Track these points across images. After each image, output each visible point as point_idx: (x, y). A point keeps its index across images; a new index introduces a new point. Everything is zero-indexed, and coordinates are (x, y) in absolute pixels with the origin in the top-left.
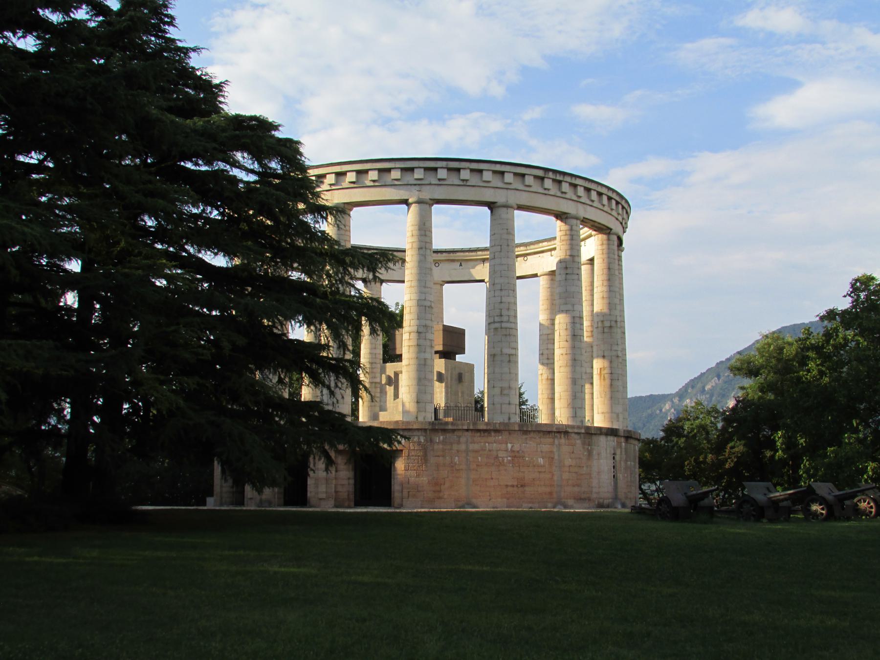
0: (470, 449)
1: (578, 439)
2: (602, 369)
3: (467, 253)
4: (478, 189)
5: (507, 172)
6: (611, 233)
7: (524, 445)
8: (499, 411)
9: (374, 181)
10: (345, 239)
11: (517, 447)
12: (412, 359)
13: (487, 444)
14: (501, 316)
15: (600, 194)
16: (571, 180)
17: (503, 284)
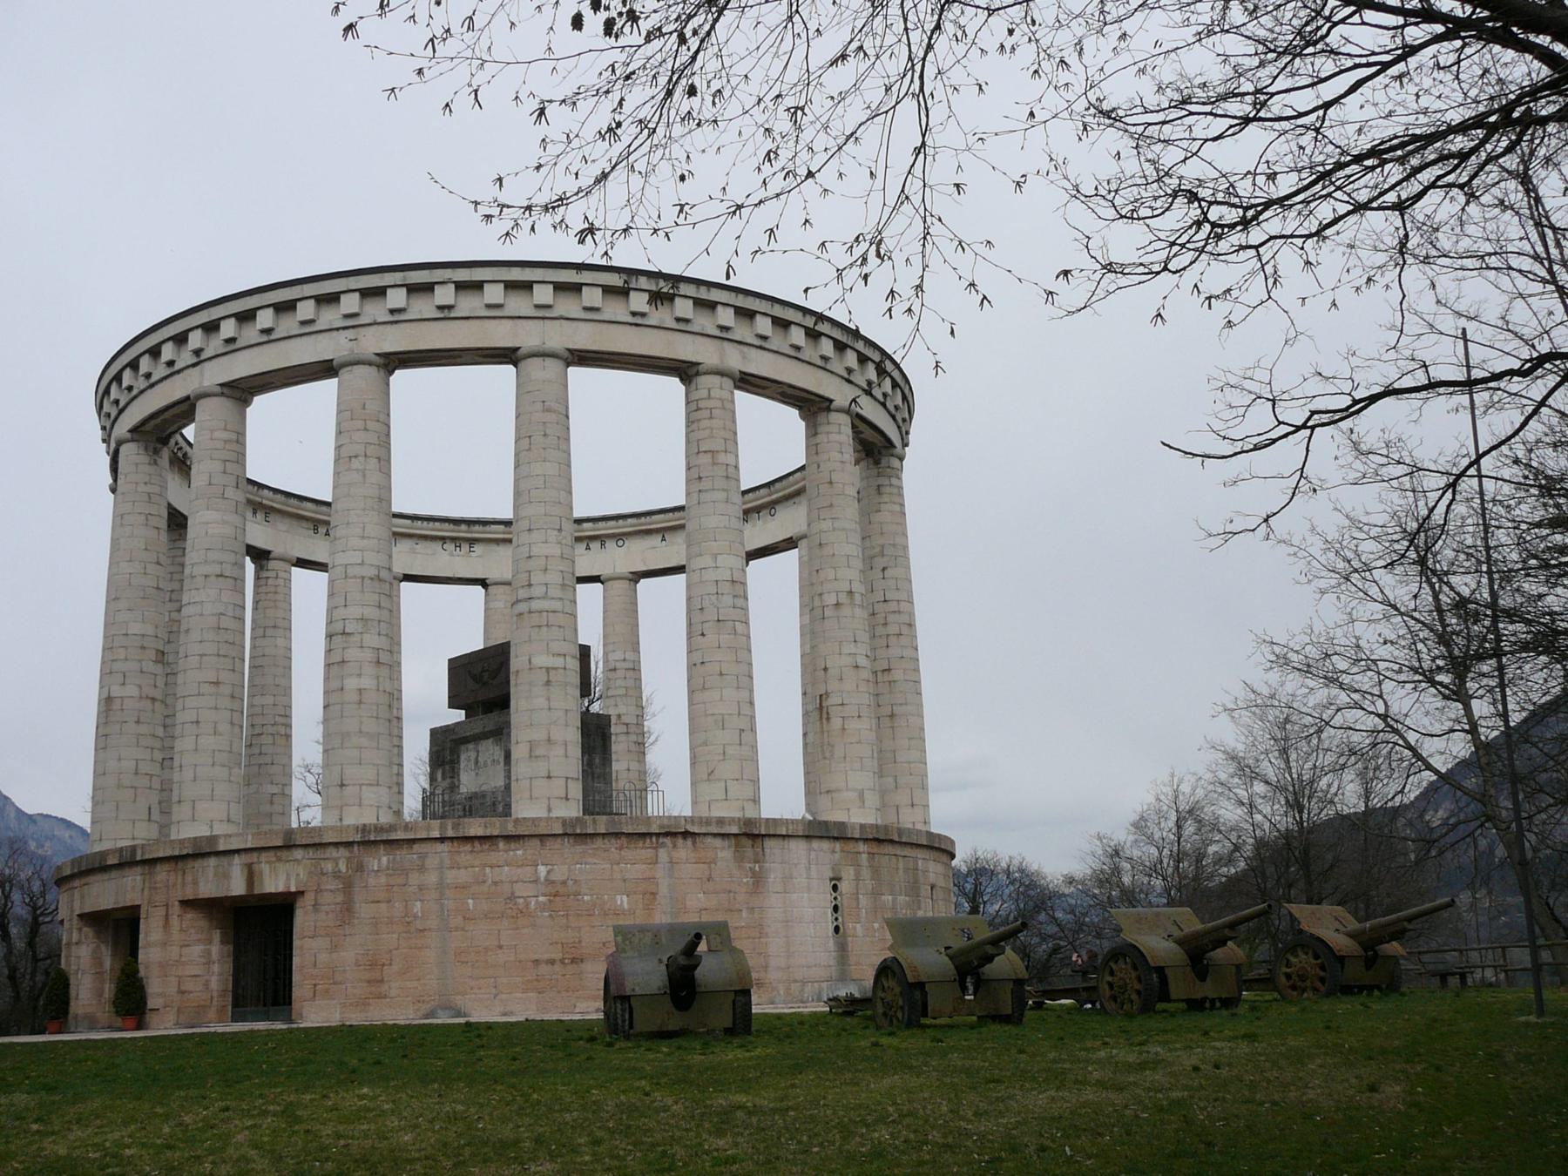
1: (723, 848)
6: (832, 407)
7: (578, 866)
8: (527, 795)
11: (560, 873)
13: (488, 870)
14: (530, 585)
16: (698, 292)
17: (533, 518)
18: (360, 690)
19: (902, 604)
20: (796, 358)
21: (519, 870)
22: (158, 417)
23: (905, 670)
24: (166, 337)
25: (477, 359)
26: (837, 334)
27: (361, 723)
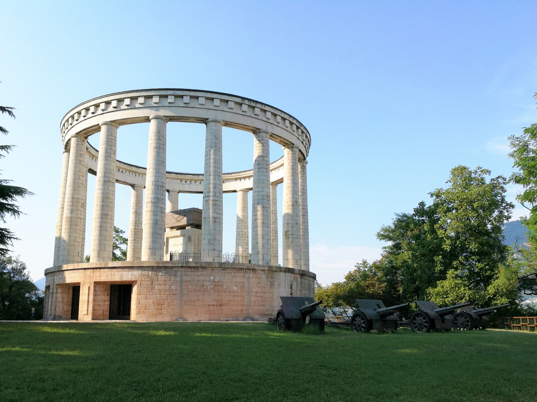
0: (184, 280)
1: (263, 274)
2: (287, 232)
3: (227, 175)
4: (196, 109)
5: (216, 98)
7: (223, 277)
8: (105, 230)
9: (128, 106)
10: (111, 144)
11: (217, 279)
12: (147, 220)
13: (196, 277)
15: (284, 119)
16: (262, 107)
18: (156, 220)
19: (305, 206)
20: (286, 130)
21: (205, 278)
22: (86, 130)
23: (305, 225)
24: (92, 105)
25: (194, 121)
26: (297, 124)
27: (156, 230)
